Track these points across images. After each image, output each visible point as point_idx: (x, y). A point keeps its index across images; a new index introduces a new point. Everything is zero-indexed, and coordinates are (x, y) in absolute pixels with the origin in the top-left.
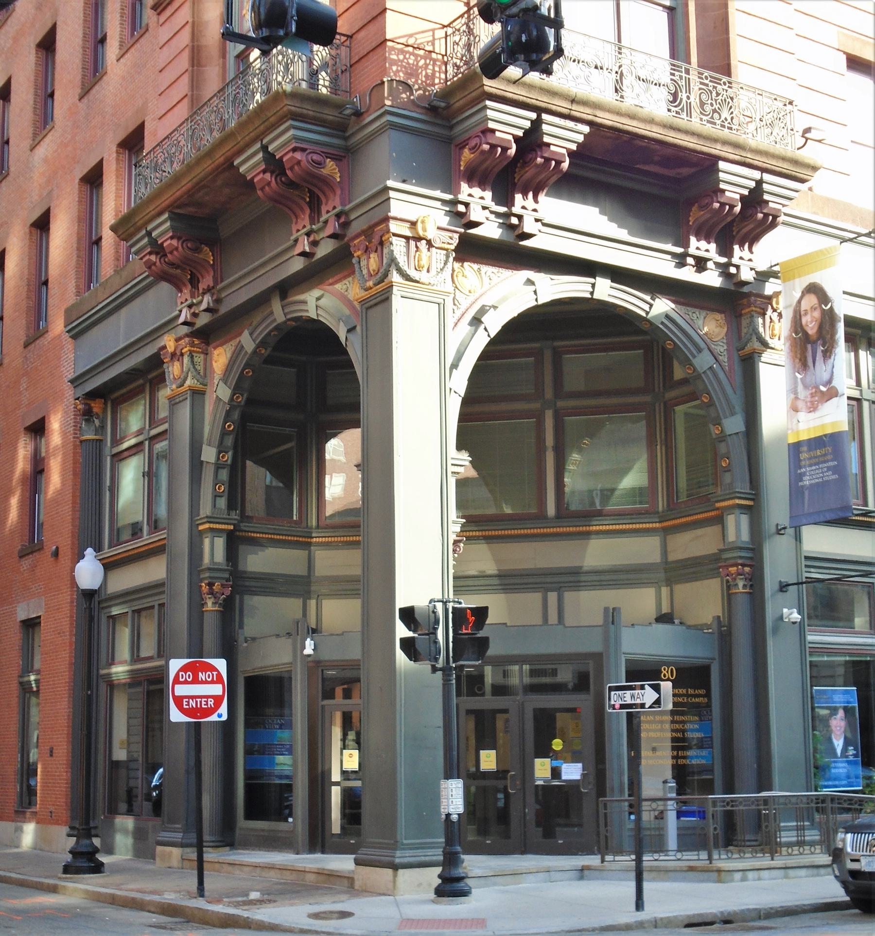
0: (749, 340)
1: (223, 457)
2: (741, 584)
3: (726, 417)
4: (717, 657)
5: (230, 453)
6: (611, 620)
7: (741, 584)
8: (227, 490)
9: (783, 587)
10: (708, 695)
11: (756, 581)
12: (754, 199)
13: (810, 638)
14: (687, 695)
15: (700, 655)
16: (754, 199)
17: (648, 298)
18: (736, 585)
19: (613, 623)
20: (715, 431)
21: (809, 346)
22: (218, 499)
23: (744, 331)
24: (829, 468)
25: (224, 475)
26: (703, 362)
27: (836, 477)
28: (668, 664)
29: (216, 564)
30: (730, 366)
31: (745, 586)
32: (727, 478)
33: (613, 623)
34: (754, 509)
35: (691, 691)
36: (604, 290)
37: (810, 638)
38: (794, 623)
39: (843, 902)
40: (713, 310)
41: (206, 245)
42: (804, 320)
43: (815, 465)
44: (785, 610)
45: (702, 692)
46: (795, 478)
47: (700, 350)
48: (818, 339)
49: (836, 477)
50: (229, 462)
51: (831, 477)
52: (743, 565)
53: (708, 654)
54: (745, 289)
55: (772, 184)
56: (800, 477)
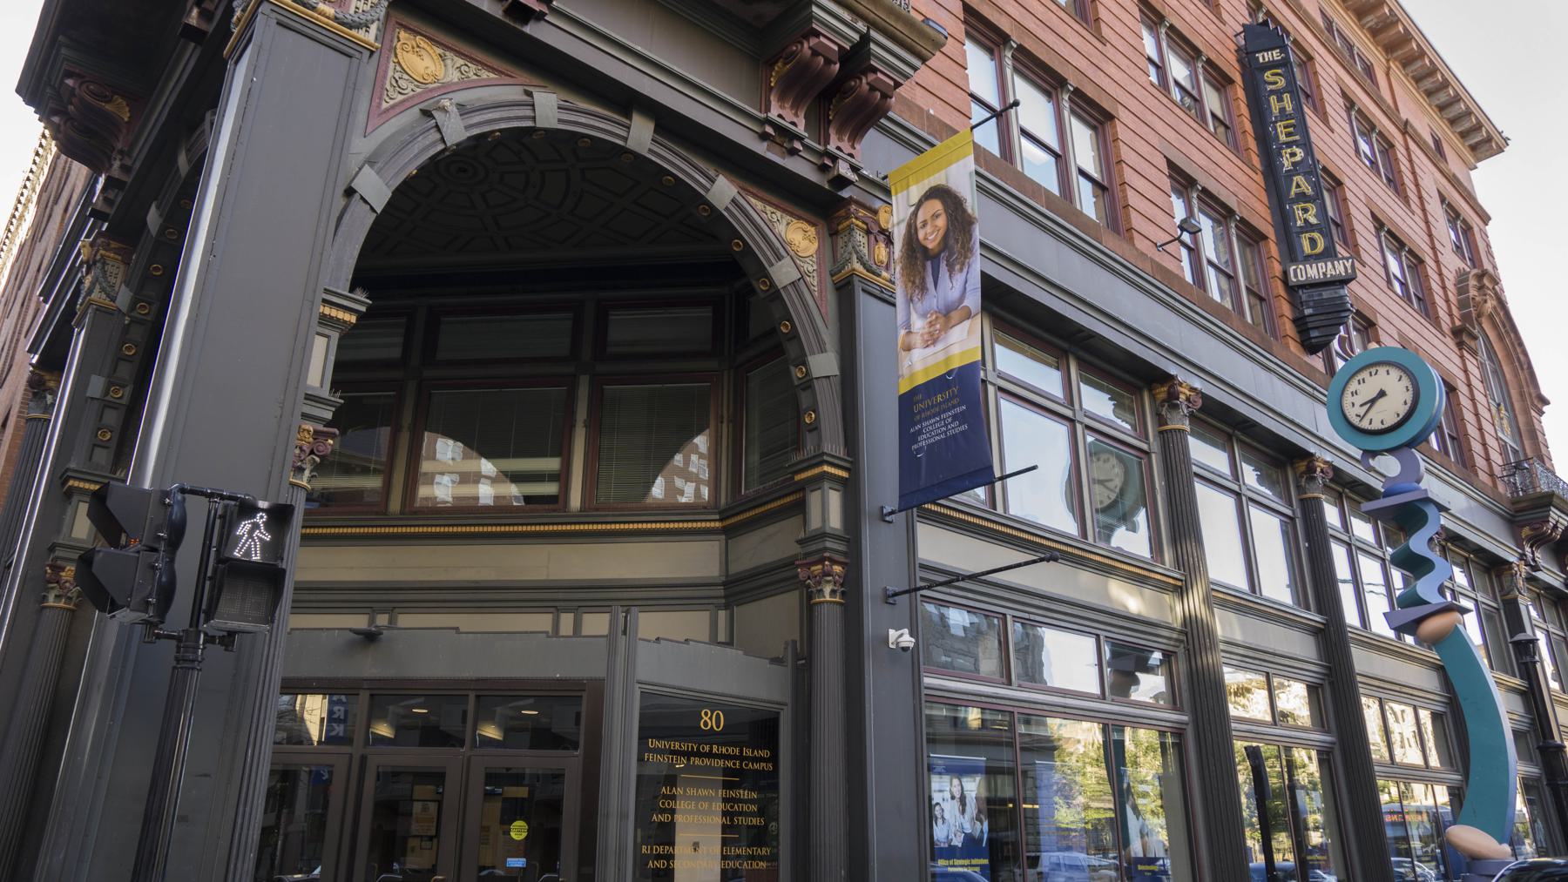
0: (849, 260)
1: (116, 392)
2: (827, 589)
3: (813, 353)
4: (789, 701)
5: (128, 390)
6: (621, 627)
7: (827, 589)
8: (115, 440)
9: (889, 598)
10: (774, 759)
11: (851, 588)
12: (856, 58)
13: (927, 681)
14: (741, 758)
15: (764, 696)
16: (856, 58)
17: (712, 173)
18: (821, 591)
19: (624, 632)
20: (797, 374)
21: (929, 264)
22: (97, 450)
23: (840, 251)
24: (955, 417)
25: (111, 418)
26: (783, 274)
27: (965, 427)
28: (713, 706)
29: (75, 540)
30: (821, 292)
31: (833, 592)
32: (810, 440)
33: (624, 632)
34: (851, 489)
35: (747, 752)
36: (640, 135)
37: (927, 681)
38: (905, 649)
39: (308, 732)
40: (799, 218)
41: (123, 97)
42: (921, 235)
43: (934, 416)
44: (892, 632)
45: (765, 753)
46: (907, 438)
47: (779, 258)
48: (943, 250)
49: (965, 427)
50: (124, 401)
51: (958, 428)
52: (834, 562)
53: (776, 697)
54: (845, 193)
55: (882, 50)
56: (914, 438)
